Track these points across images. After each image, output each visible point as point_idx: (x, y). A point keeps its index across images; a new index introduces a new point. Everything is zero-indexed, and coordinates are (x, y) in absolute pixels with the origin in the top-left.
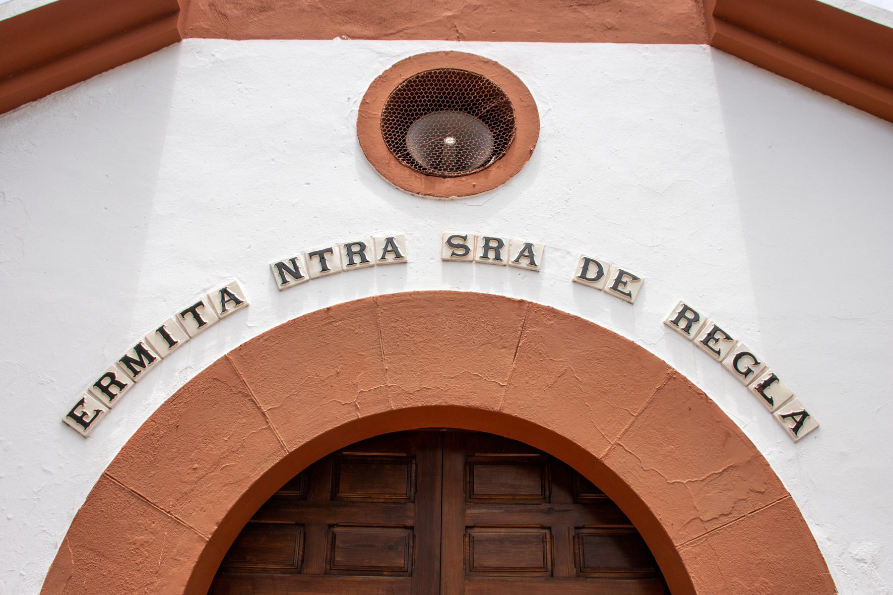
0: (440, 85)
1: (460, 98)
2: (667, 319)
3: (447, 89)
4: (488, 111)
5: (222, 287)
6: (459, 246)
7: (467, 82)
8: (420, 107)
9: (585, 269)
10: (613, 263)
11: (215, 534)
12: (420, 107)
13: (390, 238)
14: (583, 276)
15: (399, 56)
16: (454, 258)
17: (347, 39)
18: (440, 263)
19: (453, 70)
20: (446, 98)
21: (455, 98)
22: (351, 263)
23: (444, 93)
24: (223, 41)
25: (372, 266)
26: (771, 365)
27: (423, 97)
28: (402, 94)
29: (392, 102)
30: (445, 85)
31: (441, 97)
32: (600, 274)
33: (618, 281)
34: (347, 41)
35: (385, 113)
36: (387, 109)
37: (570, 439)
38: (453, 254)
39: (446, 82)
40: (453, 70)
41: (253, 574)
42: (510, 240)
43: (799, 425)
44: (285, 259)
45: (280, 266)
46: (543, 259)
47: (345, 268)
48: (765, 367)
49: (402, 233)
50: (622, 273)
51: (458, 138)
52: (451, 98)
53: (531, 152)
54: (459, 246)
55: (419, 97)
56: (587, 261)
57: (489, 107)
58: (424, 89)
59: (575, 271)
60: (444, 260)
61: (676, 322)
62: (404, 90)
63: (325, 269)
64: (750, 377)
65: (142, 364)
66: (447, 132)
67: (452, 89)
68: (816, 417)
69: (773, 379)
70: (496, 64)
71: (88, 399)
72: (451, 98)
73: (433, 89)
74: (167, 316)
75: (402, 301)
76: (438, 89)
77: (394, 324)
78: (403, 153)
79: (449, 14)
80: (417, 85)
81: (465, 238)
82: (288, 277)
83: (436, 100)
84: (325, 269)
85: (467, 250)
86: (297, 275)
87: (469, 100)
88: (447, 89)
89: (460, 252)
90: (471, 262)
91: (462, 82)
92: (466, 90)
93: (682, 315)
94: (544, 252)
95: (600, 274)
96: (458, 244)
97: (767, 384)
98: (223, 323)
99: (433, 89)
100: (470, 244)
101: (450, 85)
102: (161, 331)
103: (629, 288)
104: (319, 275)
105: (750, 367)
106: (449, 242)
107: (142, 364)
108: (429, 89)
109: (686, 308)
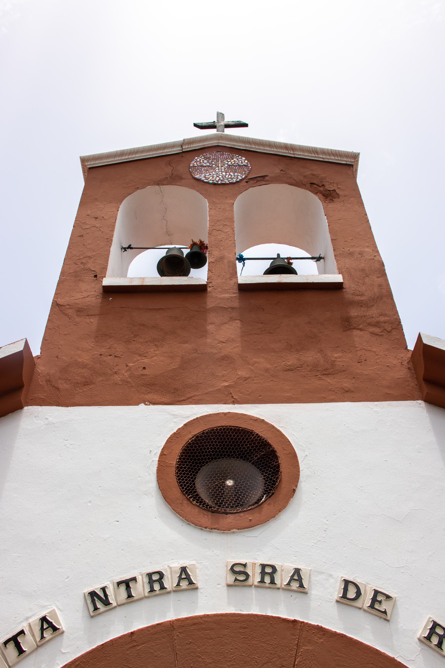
1: (237, 449)
2: (421, 635)
4: (258, 459)
6: (240, 573)
9: (346, 590)
13: (183, 567)
14: (344, 596)
15: (188, 417)
16: (237, 583)
18: (225, 588)
21: (233, 449)
22: (152, 590)
24: (55, 407)
25: (169, 593)
27: (208, 449)
28: (192, 447)
29: (184, 453)
31: (222, 448)
35: (178, 462)
36: (180, 459)
38: (236, 580)
42: (282, 566)
44: (96, 587)
45: (93, 594)
46: (309, 582)
47: (147, 594)
49: (194, 562)
50: (376, 592)
53: (294, 491)
54: (240, 573)
55: (205, 449)
56: (347, 583)
58: (209, 442)
60: (229, 586)
61: (428, 638)
62: (193, 444)
72: (229, 449)
73: (216, 442)
75: (195, 624)
77: (188, 646)
78: (193, 494)
79: (226, 384)
80: (203, 440)
81: (245, 565)
82: (99, 605)
85: (247, 575)
86: (106, 602)
89: (242, 578)
90: (251, 586)
93: (432, 631)
94: (310, 576)
95: (359, 593)
98: (41, 650)
99: (216, 442)
100: (249, 571)
104: (125, 601)
106: (232, 569)
108: (212, 442)
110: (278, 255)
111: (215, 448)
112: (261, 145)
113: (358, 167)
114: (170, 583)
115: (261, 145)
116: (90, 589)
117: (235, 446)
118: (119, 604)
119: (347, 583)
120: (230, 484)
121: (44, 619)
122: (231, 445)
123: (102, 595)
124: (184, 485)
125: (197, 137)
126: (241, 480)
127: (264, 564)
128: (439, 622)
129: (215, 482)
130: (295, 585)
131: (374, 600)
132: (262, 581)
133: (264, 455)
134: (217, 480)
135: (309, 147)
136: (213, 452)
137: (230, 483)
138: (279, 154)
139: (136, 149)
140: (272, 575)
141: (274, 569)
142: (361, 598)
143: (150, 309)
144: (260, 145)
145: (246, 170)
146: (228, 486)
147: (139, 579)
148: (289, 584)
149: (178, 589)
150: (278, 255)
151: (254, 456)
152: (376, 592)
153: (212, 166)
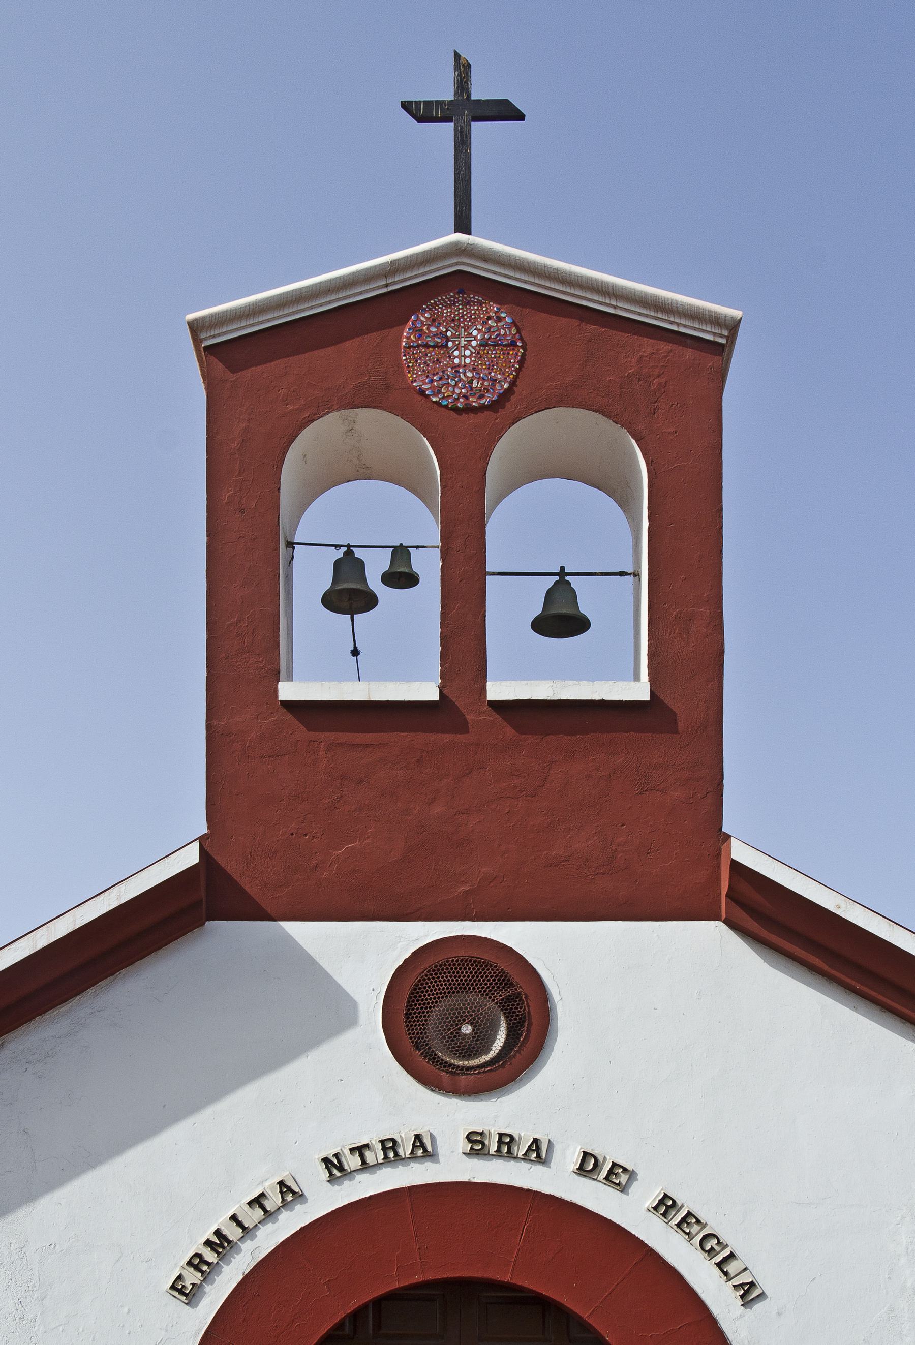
0: (458, 973)
1: (477, 985)
2: (649, 1205)
3: (464, 976)
4: (503, 999)
6: (476, 1142)
7: (483, 969)
8: (439, 995)
9: (583, 1161)
10: (610, 1154)
12: (439, 995)
13: (417, 1134)
19: (470, 958)
20: (463, 984)
21: (472, 984)
22: (203, 1272)
23: (461, 980)
26: (734, 1244)
27: (442, 985)
30: (462, 973)
31: (459, 984)
32: (596, 1165)
38: (472, 1149)
39: (463, 970)
40: (470, 958)
44: (329, 1153)
45: (326, 1161)
47: (380, 1161)
48: (727, 1245)
50: (614, 1165)
51: (475, 1026)
52: (468, 984)
54: (476, 1142)
55: (438, 985)
56: (586, 1155)
57: (504, 995)
58: (442, 977)
63: (265, 1211)
66: (464, 1020)
67: (468, 976)
69: (732, 1256)
70: (511, 950)
71: (185, 1274)
72: (468, 984)
73: (451, 976)
74: (238, 1204)
76: (455, 977)
78: (425, 1048)
81: (481, 1134)
82: (335, 1171)
83: (454, 987)
84: (265, 1211)
86: (341, 1168)
87: (492, 972)
88: (464, 976)
91: (479, 969)
92: (482, 977)
93: (661, 1202)
96: (593, 1164)
97: (726, 1260)
99: (451, 976)
101: (467, 973)
102: (234, 1218)
103: (624, 1179)
105: (713, 1246)
106: (468, 1137)
108: (447, 977)
109: (666, 1196)
110: (562, 568)
111: (450, 984)
112: (517, 267)
113: (728, 371)
115: (517, 267)
117: (475, 981)
118: (352, 1170)
120: (468, 1032)
121: (281, 1184)
122: (470, 980)
123: (335, 1161)
124: (414, 1037)
126: (480, 1025)
127: (501, 1133)
128: (187, 1259)
129: (449, 1030)
131: (611, 1172)
132: (499, 1150)
133: (510, 996)
134: (452, 1025)
136: (447, 989)
137: (467, 1029)
139: (304, 290)
142: (598, 1170)
144: (516, 269)
146: (465, 1035)
149: (413, 1157)
150: (562, 568)
151: (498, 995)
153: (447, 345)
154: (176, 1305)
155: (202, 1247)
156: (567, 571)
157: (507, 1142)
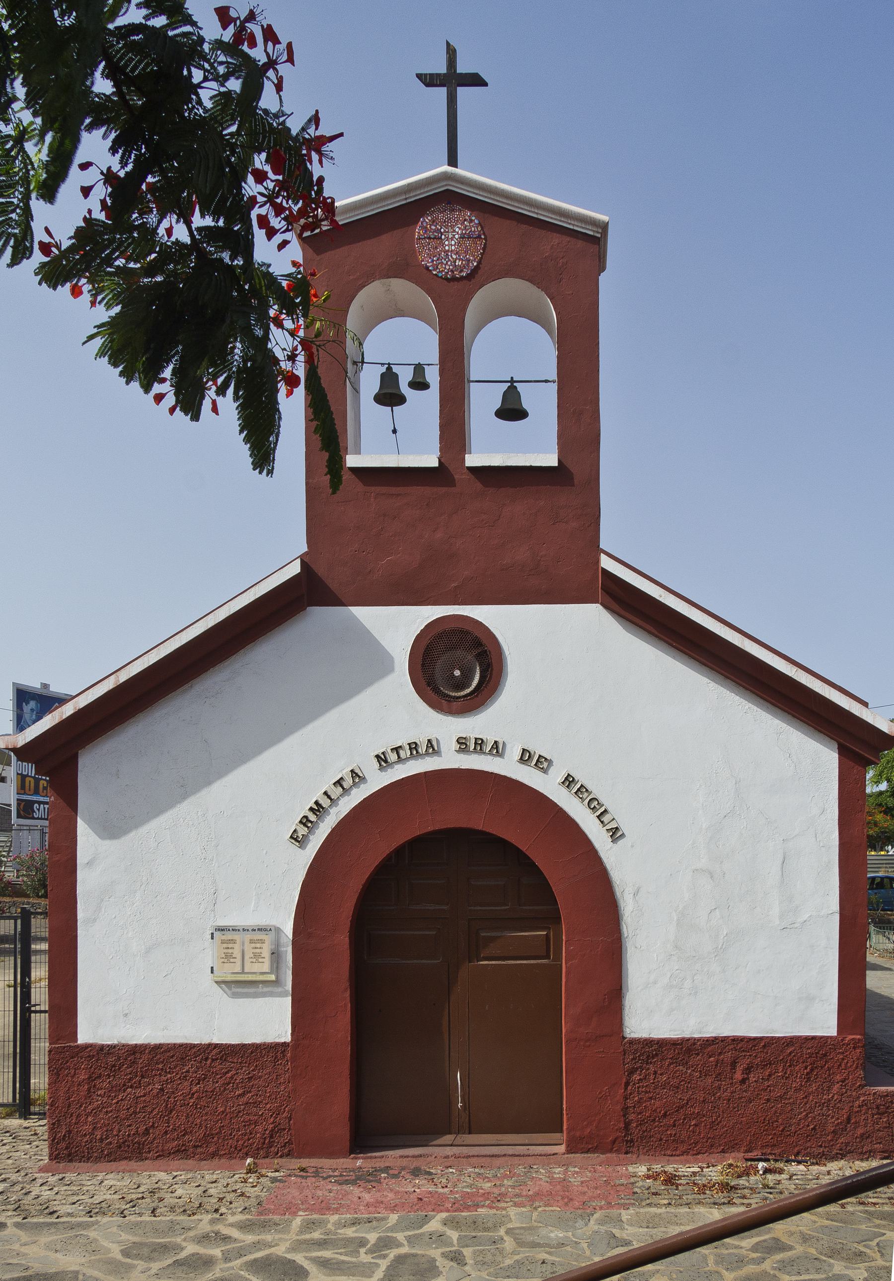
5: (497, 740)
6: (462, 743)
10: (539, 749)
11: (362, 890)
14: (521, 759)
16: (461, 750)
17: (100, 93)
26: (607, 803)
32: (529, 757)
33: (538, 761)
34: (101, 92)
37: (654, 1247)
38: (460, 748)
41: (170, 1261)
43: (614, 833)
44: (379, 751)
45: (377, 757)
50: (540, 756)
54: (462, 743)
56: (524, 750)
59: (455, 746)
61: (563, 783)
63: (331, 799)
64: (595, 810)
65: (318, 810)
68: (624, 828)
71: (298, 829)
79: (456, 584)
82: (383, 763)
86: (386, 761)
93: (566, 779)
102: (326, 793)
103: (545, 765)
107: (318, 810)
110: (512, 378)
114: (422, 749)
116: (376, 753)
119: (524, 750)
121: (352, 771)
125: (437, 174)
130: (357, 780)
135: (572, 211)
138: (520, 211)
140: (415, 748)
141: (415, 743)
143: (392, 495)
145: (185, 40)
147: (346, 777)
148: (353, 781)
150: (512, 378)
152: (540, 756)
154: (293, 848)
155: (307, 812)
156: (514, 379)
157: (480, 743)
